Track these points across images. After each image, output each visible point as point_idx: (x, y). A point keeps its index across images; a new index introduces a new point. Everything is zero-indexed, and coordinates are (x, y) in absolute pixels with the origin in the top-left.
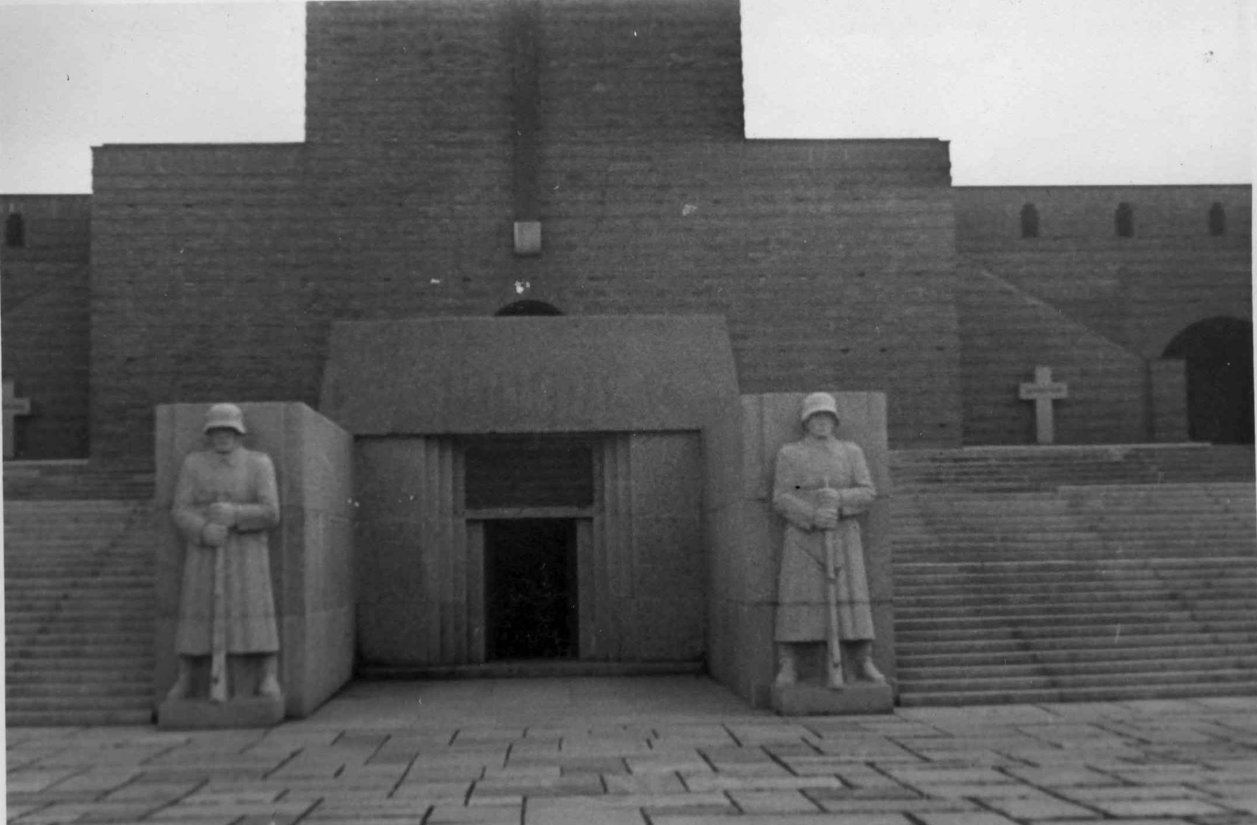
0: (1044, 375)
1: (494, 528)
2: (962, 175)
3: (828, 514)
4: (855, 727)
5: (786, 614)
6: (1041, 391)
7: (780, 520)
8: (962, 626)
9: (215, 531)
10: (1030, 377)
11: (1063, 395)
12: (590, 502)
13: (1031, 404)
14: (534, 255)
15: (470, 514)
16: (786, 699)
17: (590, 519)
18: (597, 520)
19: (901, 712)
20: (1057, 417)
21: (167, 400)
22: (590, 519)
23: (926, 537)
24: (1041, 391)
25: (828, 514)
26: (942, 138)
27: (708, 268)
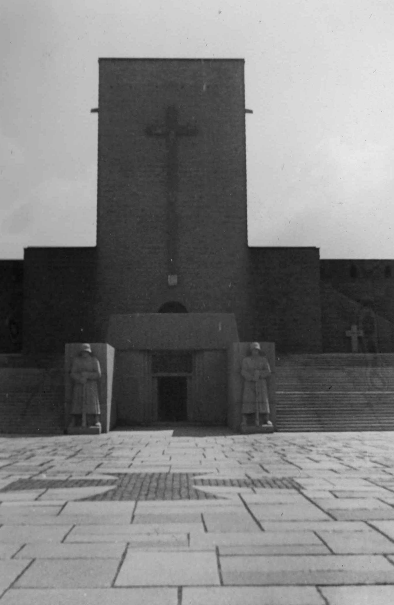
0: (354, 328)
2: (323, 256)
7: (243, 379)
10: (350, 329)
13: (350, 338)
14: (174, 287)
21: (70, 342)
23: (299, 384)
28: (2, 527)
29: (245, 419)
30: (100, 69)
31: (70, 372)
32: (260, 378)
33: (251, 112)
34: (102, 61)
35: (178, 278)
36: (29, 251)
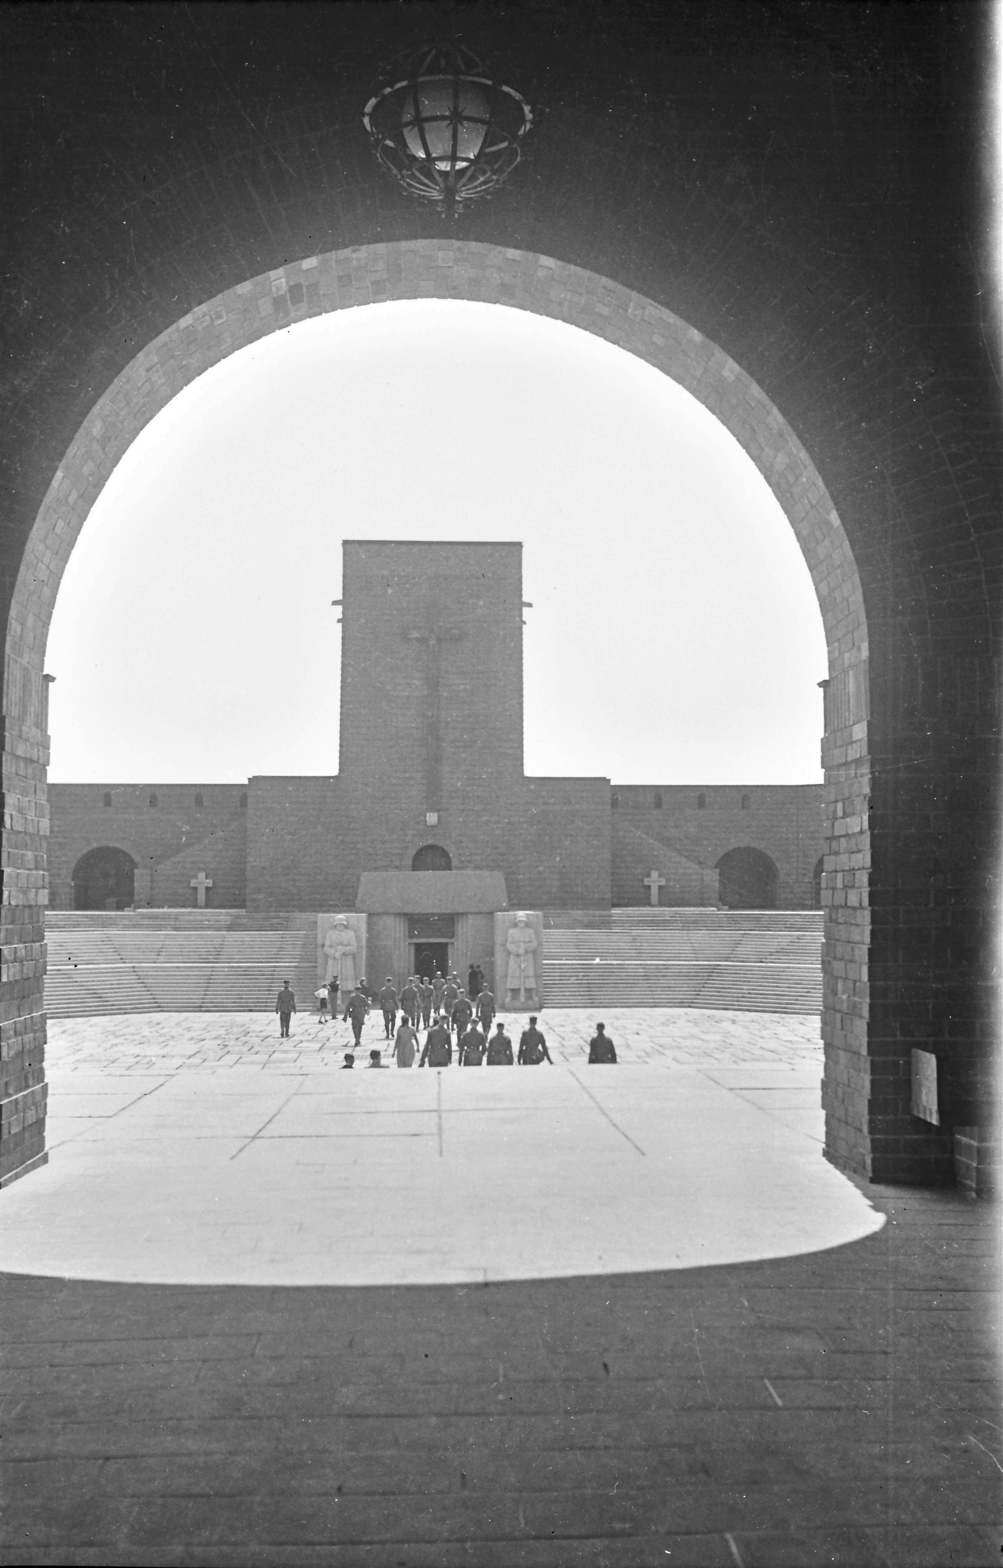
0: (655, 874)
1: (418, 947)
3: (521, 951)
4: (60, 1022)
5: (509, 979)
6: (654, 881)
8: (573, 984)
9: (337, 955)
10: (649, 875)
11: (663, 883)
12: (453, 936)
13: (649, 887)
15: (409, 941)
16: (507, 1006)
17: (453, 943)
18: (455, 943)
19: (204, 1025)
20: (660, 892)
22: (453, 943)
24: (654, 881)
25: (521, 951)
26: (608, 778)
27: (186, 1422)
28: (3, 1190)
29: (509, 994)
30: (345, 554)
31: (323, 946)
32: (526, 952)
33: (530, 605)
34: (346, 543)
35: (439, 817)
36: (254, 780)
